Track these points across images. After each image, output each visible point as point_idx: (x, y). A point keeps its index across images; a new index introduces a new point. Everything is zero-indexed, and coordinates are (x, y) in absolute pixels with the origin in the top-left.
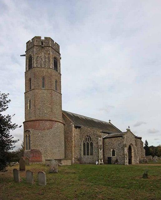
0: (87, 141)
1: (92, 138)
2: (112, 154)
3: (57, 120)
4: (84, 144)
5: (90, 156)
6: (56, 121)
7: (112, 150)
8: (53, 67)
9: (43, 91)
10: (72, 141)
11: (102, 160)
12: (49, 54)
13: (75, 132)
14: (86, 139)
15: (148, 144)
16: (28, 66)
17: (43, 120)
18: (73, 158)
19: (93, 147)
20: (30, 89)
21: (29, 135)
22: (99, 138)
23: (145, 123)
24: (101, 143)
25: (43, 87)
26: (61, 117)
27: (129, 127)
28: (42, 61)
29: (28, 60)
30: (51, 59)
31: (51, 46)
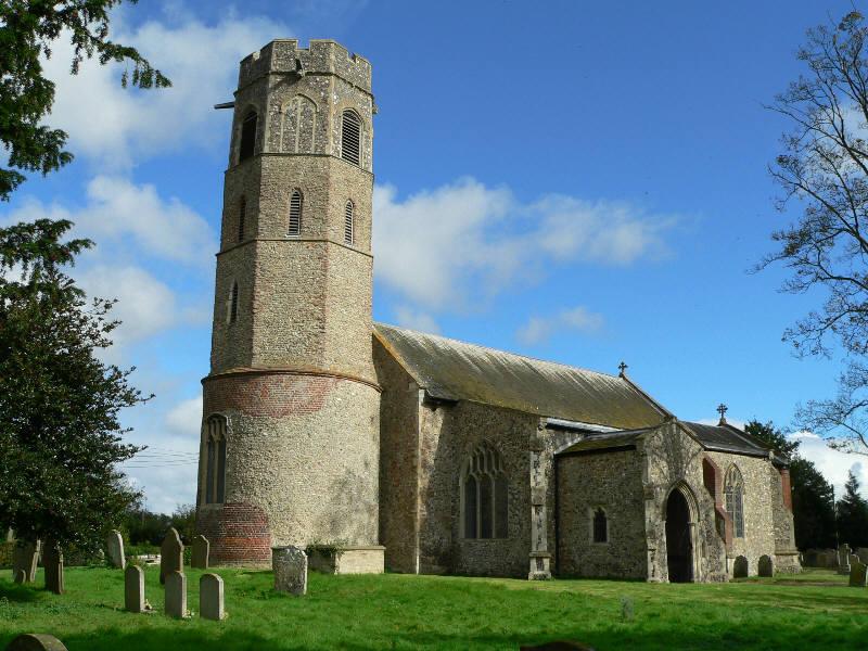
0: (482, 469)
1: (504, 454)
2: (592, 534)
3: (346, 372)
4: (471, 483)
5: (495, 543)
6: (340, 377)
7: (591, 513)
8: (340, 147)
9: (292, 246)
10: (415, 467)
11: (546, 562)
12: (325, 101)
13: (430, 426)
14: (479, 459)
15: (857, 486)
16: (237, 148)
17: (284, 372)
18: (418, 552)
19: (510, 497)
20: (241, 237)
21: (223, 437)
22: (533, 457)
23: (86, 243)
24: (539, 478)
25: (293, 229)
26: (368, 355)
27: (722, 409)
28: (295, 128)
29: (240, 126)
30: (331, 120)
31: (333, 70)
